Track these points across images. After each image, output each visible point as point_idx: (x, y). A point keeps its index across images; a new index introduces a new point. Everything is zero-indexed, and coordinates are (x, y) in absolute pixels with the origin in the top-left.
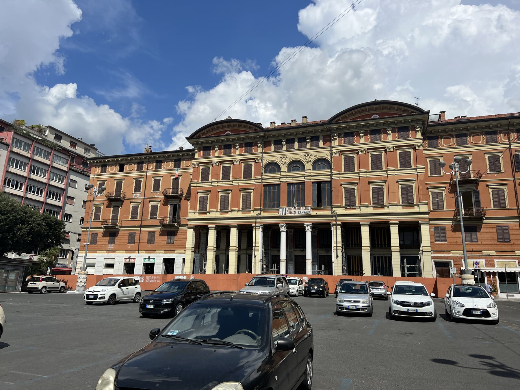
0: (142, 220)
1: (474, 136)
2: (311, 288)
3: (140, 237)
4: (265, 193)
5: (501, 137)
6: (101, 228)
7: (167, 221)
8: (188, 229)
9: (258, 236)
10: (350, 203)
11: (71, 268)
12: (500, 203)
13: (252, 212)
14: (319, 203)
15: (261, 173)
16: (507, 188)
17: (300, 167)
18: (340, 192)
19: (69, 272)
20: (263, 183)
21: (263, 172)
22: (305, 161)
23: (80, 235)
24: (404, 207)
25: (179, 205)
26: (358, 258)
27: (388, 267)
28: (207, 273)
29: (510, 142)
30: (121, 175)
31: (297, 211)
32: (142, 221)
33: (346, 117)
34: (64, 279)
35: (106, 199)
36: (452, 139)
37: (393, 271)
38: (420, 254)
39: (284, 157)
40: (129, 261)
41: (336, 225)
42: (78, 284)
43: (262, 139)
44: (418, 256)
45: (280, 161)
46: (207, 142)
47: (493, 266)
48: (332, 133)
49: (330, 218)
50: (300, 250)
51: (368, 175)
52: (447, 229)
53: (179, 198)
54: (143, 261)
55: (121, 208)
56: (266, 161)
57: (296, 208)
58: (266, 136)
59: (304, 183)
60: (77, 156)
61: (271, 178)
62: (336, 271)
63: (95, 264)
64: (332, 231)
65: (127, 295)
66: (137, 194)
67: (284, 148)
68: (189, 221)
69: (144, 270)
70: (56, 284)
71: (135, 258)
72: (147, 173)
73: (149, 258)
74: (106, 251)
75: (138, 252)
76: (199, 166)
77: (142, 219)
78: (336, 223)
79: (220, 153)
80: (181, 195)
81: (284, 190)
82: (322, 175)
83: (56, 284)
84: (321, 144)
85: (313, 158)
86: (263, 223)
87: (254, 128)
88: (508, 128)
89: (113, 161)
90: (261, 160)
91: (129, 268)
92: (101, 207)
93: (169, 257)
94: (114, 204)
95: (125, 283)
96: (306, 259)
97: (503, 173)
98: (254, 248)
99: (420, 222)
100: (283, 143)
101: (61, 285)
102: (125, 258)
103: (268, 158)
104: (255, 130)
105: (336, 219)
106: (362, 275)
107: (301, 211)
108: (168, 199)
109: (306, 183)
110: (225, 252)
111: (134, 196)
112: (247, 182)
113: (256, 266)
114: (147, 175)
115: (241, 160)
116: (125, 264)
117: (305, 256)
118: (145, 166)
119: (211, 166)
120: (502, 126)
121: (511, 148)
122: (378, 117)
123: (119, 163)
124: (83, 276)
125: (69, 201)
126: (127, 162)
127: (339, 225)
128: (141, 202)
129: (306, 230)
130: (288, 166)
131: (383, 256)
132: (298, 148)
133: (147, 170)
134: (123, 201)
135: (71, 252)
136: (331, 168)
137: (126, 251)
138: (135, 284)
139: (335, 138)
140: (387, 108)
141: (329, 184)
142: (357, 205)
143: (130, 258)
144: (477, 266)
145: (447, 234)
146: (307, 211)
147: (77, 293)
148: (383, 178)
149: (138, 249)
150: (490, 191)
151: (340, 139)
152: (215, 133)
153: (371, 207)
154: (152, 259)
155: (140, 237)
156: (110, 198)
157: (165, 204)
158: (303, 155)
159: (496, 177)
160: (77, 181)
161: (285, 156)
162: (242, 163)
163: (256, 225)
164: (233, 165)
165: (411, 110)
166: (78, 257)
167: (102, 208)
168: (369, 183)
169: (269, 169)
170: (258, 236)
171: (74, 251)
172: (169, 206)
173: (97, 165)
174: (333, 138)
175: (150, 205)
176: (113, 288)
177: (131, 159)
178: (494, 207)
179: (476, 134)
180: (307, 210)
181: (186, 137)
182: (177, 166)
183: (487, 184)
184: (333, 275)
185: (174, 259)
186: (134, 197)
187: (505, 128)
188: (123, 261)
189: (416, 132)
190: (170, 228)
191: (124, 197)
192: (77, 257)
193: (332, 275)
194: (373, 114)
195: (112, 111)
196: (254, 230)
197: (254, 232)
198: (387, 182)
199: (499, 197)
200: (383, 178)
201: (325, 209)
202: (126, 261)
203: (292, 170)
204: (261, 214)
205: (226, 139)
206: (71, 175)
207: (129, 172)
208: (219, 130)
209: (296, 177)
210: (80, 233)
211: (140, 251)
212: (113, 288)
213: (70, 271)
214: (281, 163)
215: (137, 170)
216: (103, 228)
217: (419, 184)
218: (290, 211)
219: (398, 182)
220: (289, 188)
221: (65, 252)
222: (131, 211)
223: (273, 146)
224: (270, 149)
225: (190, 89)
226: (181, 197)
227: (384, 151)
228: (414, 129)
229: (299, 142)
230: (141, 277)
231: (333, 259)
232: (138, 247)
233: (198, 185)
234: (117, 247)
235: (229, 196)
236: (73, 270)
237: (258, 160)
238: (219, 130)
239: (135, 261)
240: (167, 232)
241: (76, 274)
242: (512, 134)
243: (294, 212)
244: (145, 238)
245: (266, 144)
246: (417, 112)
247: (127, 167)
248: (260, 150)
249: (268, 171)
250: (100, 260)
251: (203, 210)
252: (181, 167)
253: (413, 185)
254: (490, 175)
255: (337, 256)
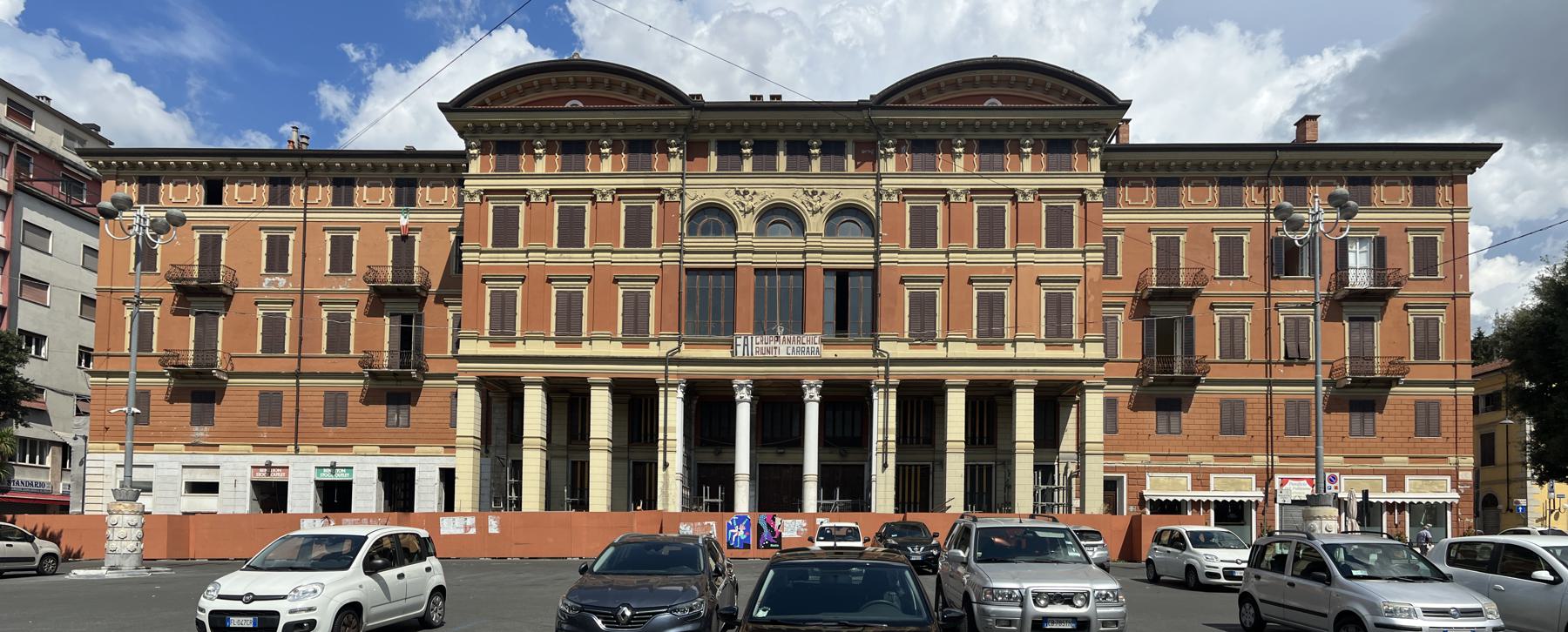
0: (300, 357)
1: (1195, 185)
2: (910, 548)
3: (297, 406)
4: (691, 292)
5: (1251, 193)
6: (161, 375)
7: (384, 362)
8: (459, 386)
9: (672, 412)
10: (923, 331)
11: (67, 494)
12: (1232, 350)
13: (653, 344)
14: (842, 324)
15: (681, 234)
16: (1250, 314)
17: (791, 226)
18: (898, 300)
19: (63, 508)
20: (685, 265)
21: (685, 231)
22: (806, 210)
23: (83, 399)
24: (1049, 345)
25: (420, 319)
26: (916, 470)
27: (985, 490)
28: (526, 507)
29: (1268, 208)
30: (214, 215)
31: (784, 348)
32: (297, 359)
33: (920, 95)
34: (47, 525)
35: (169, 286)
36: (1147, 188)
37: (590, 498)
38: (1058, 459)
39: (746, 193)
40: (269, 474)
41: (887, 386)
42: (111, 545)
43: (681, 132)
44: (1054, 466)
45: (734, 203)
46: (510, 128)
47: (1206, 487)
48: (880, 137)
49: (871, 368)
50: (774, 451)
51: (969, 259)
52: (1120, 404)
53: (417, 296)
54: (314, 475)
55: (223, 316)
56: (695, 201)
57: (782, 337)
58: (696, 125)
59: (732, 272)
60: (37, 152)
61: (708, 251)
62: (880, 502)
63: (151, 483)
64: (875, 403)
65: (402, 604)
66: (277, 278)
67: (747, 166)
68: (460, 362)
69: (319, 502)
70: (22, 548)
71: (288, 467)
72: (305, 215)
73: (333, 467)
74: (185, 445)
75: (297, 450)
76: (484, 201)
77: (300, 352)
78: (887, 382)
79: (549, 165)
80: (425, 288)
81: (746, 286)
82: (852, 250)
83: (22, 548)
84: (850, 164)
85: (828, 203)
86: (688, 377)
87: (658, 97)
88: (1269, 174)
89: (180, 166)
90: (678, 195)
91: (268, 496)
92: (153, 313)
93: (395, 464)
94: (198, 304)
95: (390, 554)
96: (734, 471)
97: (1246, 279)
98: (661, 443)
99: (1084, 383)
100: (744, 151)
101: (42, 551)
102: (252, 467)
103: (700, 193)
104: (662, 101)
105: (887, 371)
106: (944, 511)
107: (796, 346)
108: (381, 298)
109: (808, 273)
110: (565, 453)
111: (267, 283)
112: (637, 258)
113: (669, 492)
114: (305, 222)
115: (618, 191)
116: (256, 485)
117: (733, 466)
118: (297, 192)
119: (524, 202)
120: (1259, 166)
121: (1269, 222)
122: (1000, 104)
123: (204, 177)
124: (126, 518)
125: (28, 292)
126: (232, 173)
127: (892, 386)
128: (292, 303)
129: (807, 397)
130: (758, 221)
131: (975, 466)
132: (717, 170)
133: (306, 204)
134: (231, 297)
135: (58, 450)
136: (875, 234)
137: (254, 445)
138: (421, 557)
139: (888, 150)
140: (1025, 81)
141: (869, 279)
142: (939, 336)
143: (269, 466)
144: (1333, 486)
145: (1120, 415)
146: (810, 346)
147: (113, 575)
148: (1004, 271)
149: (296, 442)
150: (1217, 319)
151: (902, 155)
152: (545, 99)
153: (973, 341)
154: (342, 470)
155: (297, 406)
156: (184, 283)
157: (374, 310)
158: (800, 193)
159: (1231, 289)
160: (50, 232)
161: (751, 191)
162: (622, 201)
163: (666, 380)
164: (593, 204)
165: (1085, 95)
166: (87, 462)
167: (157, 314)
168: (970, 282)
169: (701, 225)
170: (672, 412)
171: (71, 443)
172: (387, 320)
173: (122, 177)
174: (882, 152)
175: (325, 314)
176: (345, 579)
177: (246, 167)
178: (1221, 357)
179: (1199, 183)
180: (811, 344)
181: (439, 104)
182: (406, 200)
183: (1211, 304)
184: (873, 510)
185: (413, 470)
186: (268, 285)
187: (1263, 173)
188: (248, 476)
189: (1090, 155)
190: (395, 383)
191: (233, 285)
192: (83, 462)
193: (870, 510)
194: (988, 96)
195: (124, 80)
196: (662, 395)
197: (661, 400)
198: (1014, 282)
199: (1232, 330)
200: (1004, 271)
201: (858, 344)
202: (259, 475)
203: (699, 230)
204: (679, 351)
205: (570, 121)
206: (24, 208)
207: (241, 206)
208: (548, 94)
209: (780, 249)
210: (86, 392)
211: (301, 448)
212: (345, 579)
213: (64, 504)
214: (738, 210)
215: (270, 203)
216: (167, 377)
217: (1089, 292)
218: (764, 345)
219: (1039, 281)
220: (759, 284)
221: (36, 448)
222: (260, 330)
223: (713, 159)
224: (705, 166)
225: (353, 53)
226: (425, 295)
227: (1011, 199)
228: (1085, 149)
229: (789, 153)
230: (326, 520)
231: (874, 472)
232: (294, 435)
233: (549, 258)
234: (223, 434)
235: (582, 296)
236: (74, 499)
237: (671, 195)
238: (544, 92)
239: (287, 475)
240: (385, 394)
241: (86, 513)
242: (1274, 188)
243: (775, 348)
244: (316, 410)
245: (695, 151)
246: (1099, 103)
247: (231, 192)
248: (675, 165)
249: (699, 230)
250: (166, 473)
251: (503, 329)
252: (419, 205)
253: (1074, 291)
254: (1219, 282)
255: (885, 466)
